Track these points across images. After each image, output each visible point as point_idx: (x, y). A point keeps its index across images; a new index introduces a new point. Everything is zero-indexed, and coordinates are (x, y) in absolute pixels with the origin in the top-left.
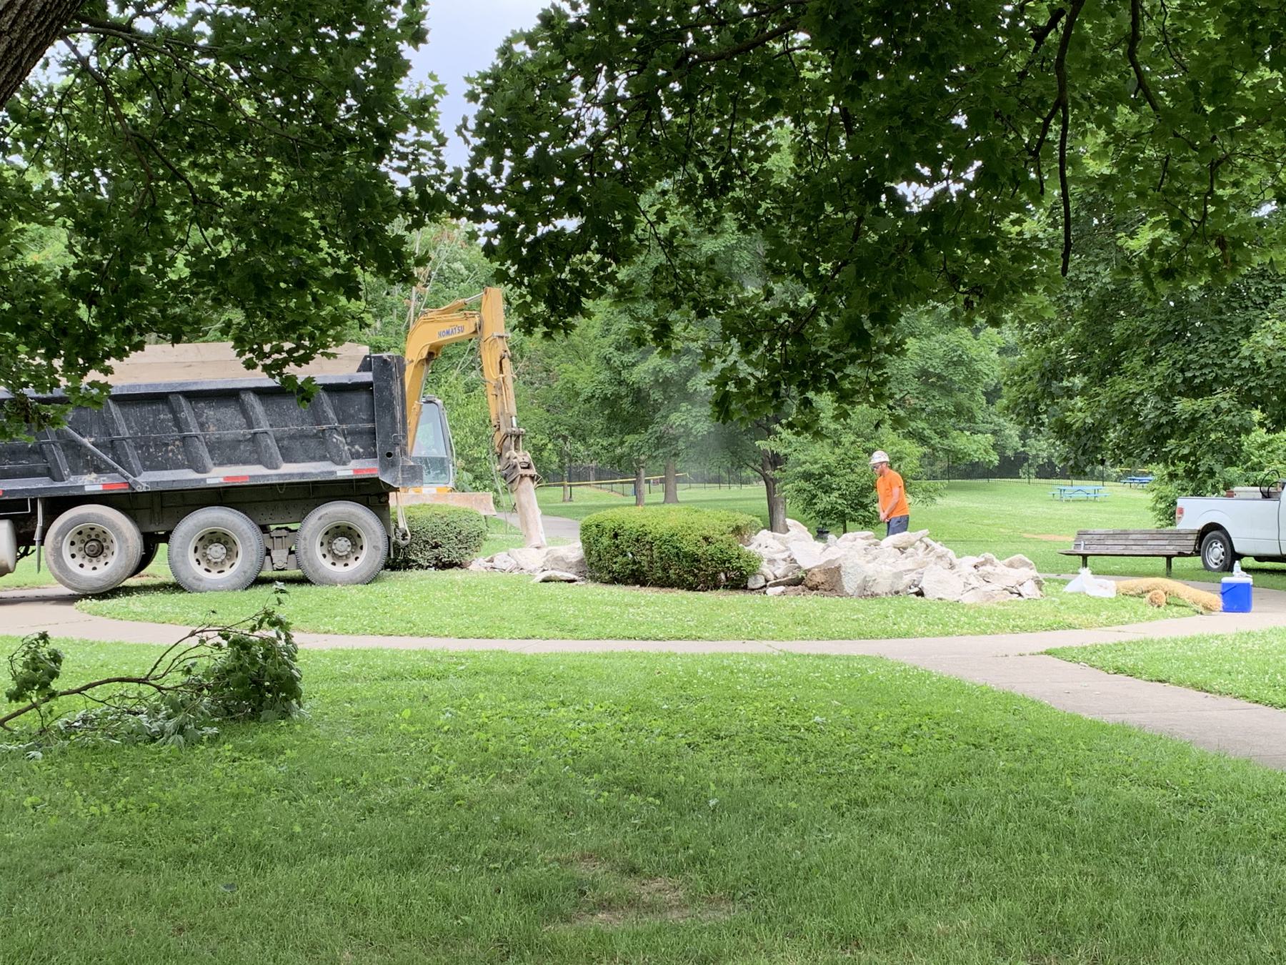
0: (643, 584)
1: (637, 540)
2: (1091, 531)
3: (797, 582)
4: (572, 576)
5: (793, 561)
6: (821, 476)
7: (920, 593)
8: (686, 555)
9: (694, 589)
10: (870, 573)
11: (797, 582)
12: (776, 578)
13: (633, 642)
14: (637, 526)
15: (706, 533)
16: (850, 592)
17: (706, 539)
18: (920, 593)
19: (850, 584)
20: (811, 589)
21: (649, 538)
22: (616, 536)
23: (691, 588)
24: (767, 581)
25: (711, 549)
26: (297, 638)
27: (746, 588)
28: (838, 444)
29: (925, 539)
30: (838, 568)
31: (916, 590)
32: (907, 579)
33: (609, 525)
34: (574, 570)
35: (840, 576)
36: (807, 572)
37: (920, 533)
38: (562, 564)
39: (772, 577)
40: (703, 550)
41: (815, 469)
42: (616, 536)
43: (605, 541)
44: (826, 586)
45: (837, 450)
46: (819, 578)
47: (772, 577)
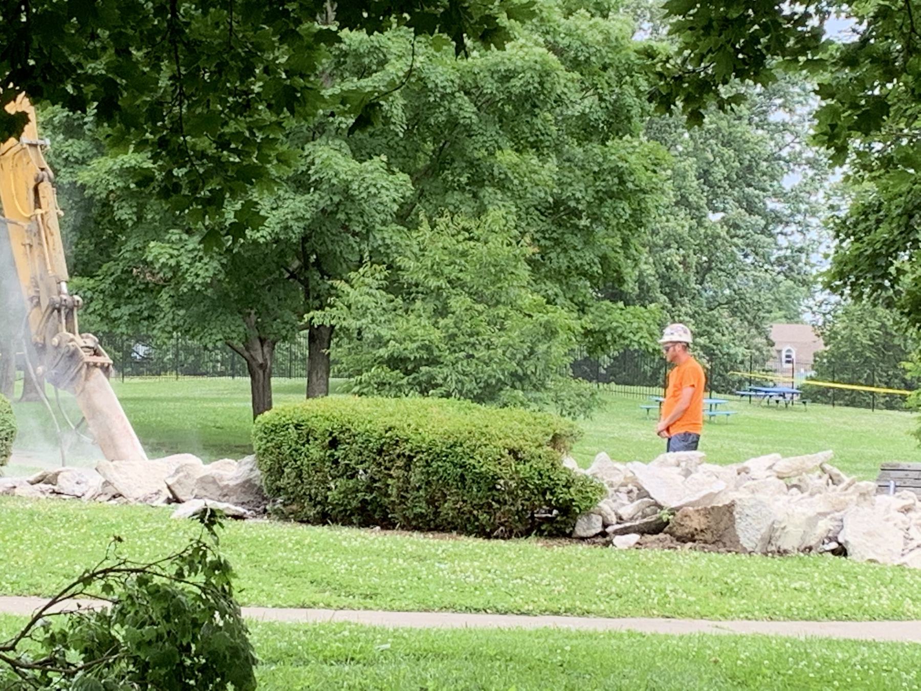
0: (387, 524)
1: (380, 452)
2: (904, 464)
3: (657, 528)
4: (241, 510)
5: (643, 493)
6: (418, 363)
7: (841, 551)
8: (480, 478)
9: (488, 536)
10: (780, 517)
11: (657, 528)
12: (620, 519)
13: (482, 616)
14: (380, 429)
15: (515, 445)
16: (749, 546)
17: (513, 452)
18: (841, 551)
19: (748, 532)
20: (682, 540)
21: (406, 448)
22: (334, 444)
23: (486, 534)
24: (605, 525)
25: (524, 469)
26: (246, 614)
27: (569, 536)
28: (442, 311)
29: (827, 467)
30: (730, 508)
31: (834, 545)
32: (824, 526)
33: (321, 426)
34: (234, 498)
35: (732, 520)
36: (673, 512)
37: (821, 456)
38: (212, 488)
39: (614, 519)
40: (508, 474)
41: (410, 349)
42: (334, 444)
43: (315, 452)
44: (708, 536)
45: (442, 322)
46: (696, 522)
47: (613, 519)
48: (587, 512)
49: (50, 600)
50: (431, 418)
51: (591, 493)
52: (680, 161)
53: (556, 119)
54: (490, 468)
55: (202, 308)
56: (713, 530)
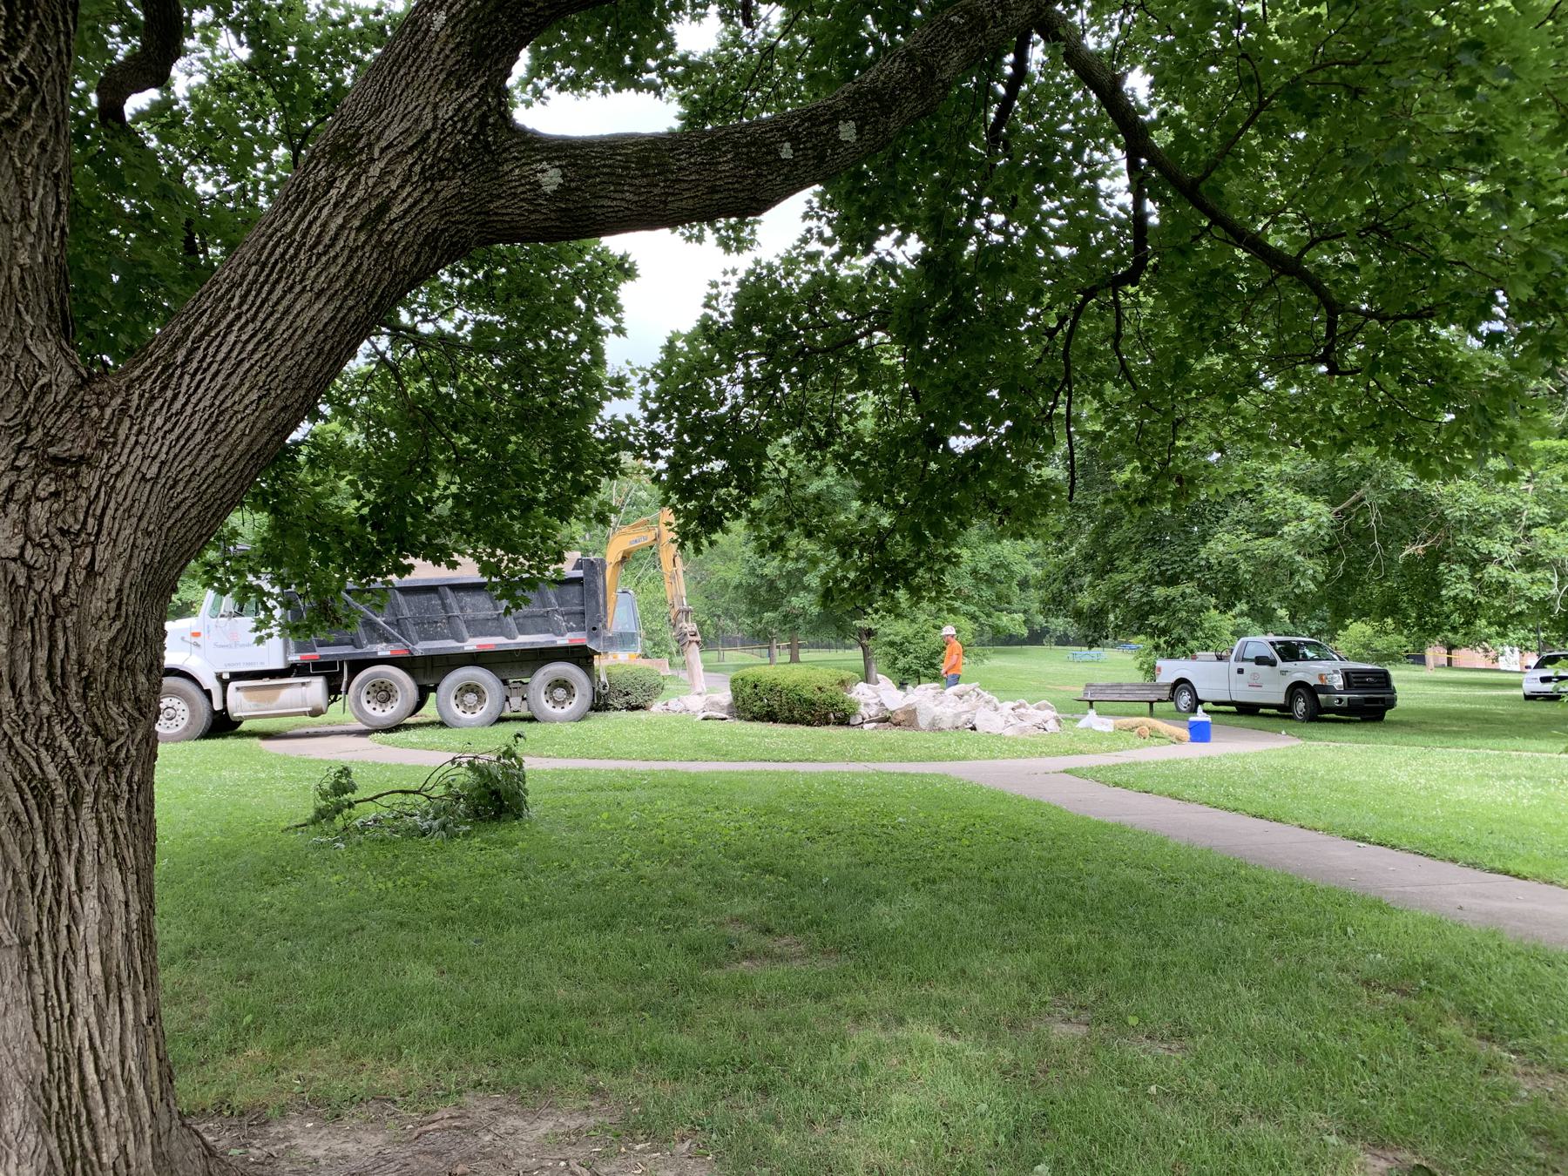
3: (886, 720)
7: (974, 728)
11: (886, 720)
18: (974, 728)
19: (923, 721)
23: (809, 724)
25: (824, 696)
33: (750, 679)
43: (748, 690)
46: (901, 717)
48: (854, 714)
49: (365, 727)
50: (1494, 693)
51: (854, 706)
52: (442, 50)
53: (1527, 109)
54: (808, 695)
55: (817, 626)
56: (908, 720)
